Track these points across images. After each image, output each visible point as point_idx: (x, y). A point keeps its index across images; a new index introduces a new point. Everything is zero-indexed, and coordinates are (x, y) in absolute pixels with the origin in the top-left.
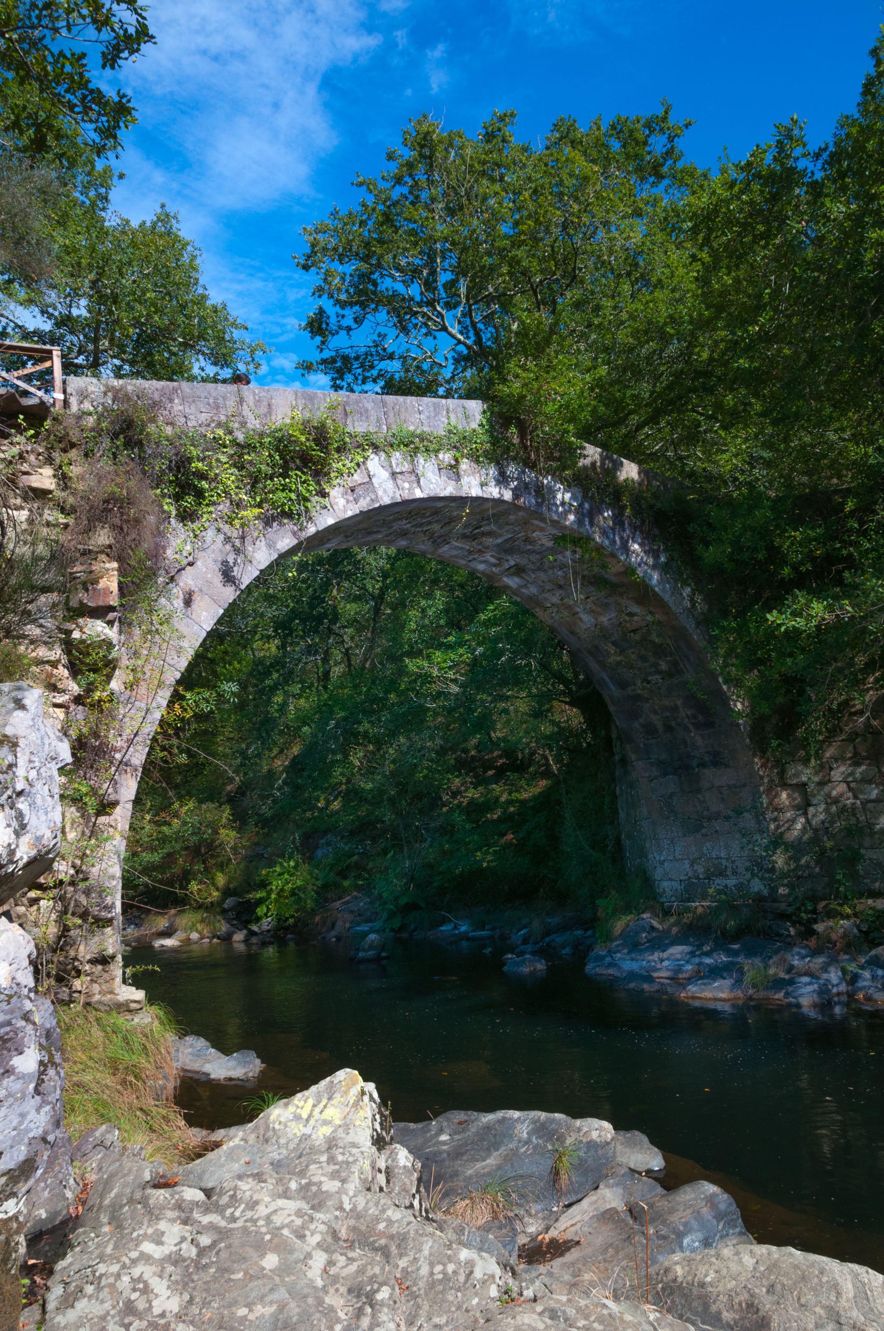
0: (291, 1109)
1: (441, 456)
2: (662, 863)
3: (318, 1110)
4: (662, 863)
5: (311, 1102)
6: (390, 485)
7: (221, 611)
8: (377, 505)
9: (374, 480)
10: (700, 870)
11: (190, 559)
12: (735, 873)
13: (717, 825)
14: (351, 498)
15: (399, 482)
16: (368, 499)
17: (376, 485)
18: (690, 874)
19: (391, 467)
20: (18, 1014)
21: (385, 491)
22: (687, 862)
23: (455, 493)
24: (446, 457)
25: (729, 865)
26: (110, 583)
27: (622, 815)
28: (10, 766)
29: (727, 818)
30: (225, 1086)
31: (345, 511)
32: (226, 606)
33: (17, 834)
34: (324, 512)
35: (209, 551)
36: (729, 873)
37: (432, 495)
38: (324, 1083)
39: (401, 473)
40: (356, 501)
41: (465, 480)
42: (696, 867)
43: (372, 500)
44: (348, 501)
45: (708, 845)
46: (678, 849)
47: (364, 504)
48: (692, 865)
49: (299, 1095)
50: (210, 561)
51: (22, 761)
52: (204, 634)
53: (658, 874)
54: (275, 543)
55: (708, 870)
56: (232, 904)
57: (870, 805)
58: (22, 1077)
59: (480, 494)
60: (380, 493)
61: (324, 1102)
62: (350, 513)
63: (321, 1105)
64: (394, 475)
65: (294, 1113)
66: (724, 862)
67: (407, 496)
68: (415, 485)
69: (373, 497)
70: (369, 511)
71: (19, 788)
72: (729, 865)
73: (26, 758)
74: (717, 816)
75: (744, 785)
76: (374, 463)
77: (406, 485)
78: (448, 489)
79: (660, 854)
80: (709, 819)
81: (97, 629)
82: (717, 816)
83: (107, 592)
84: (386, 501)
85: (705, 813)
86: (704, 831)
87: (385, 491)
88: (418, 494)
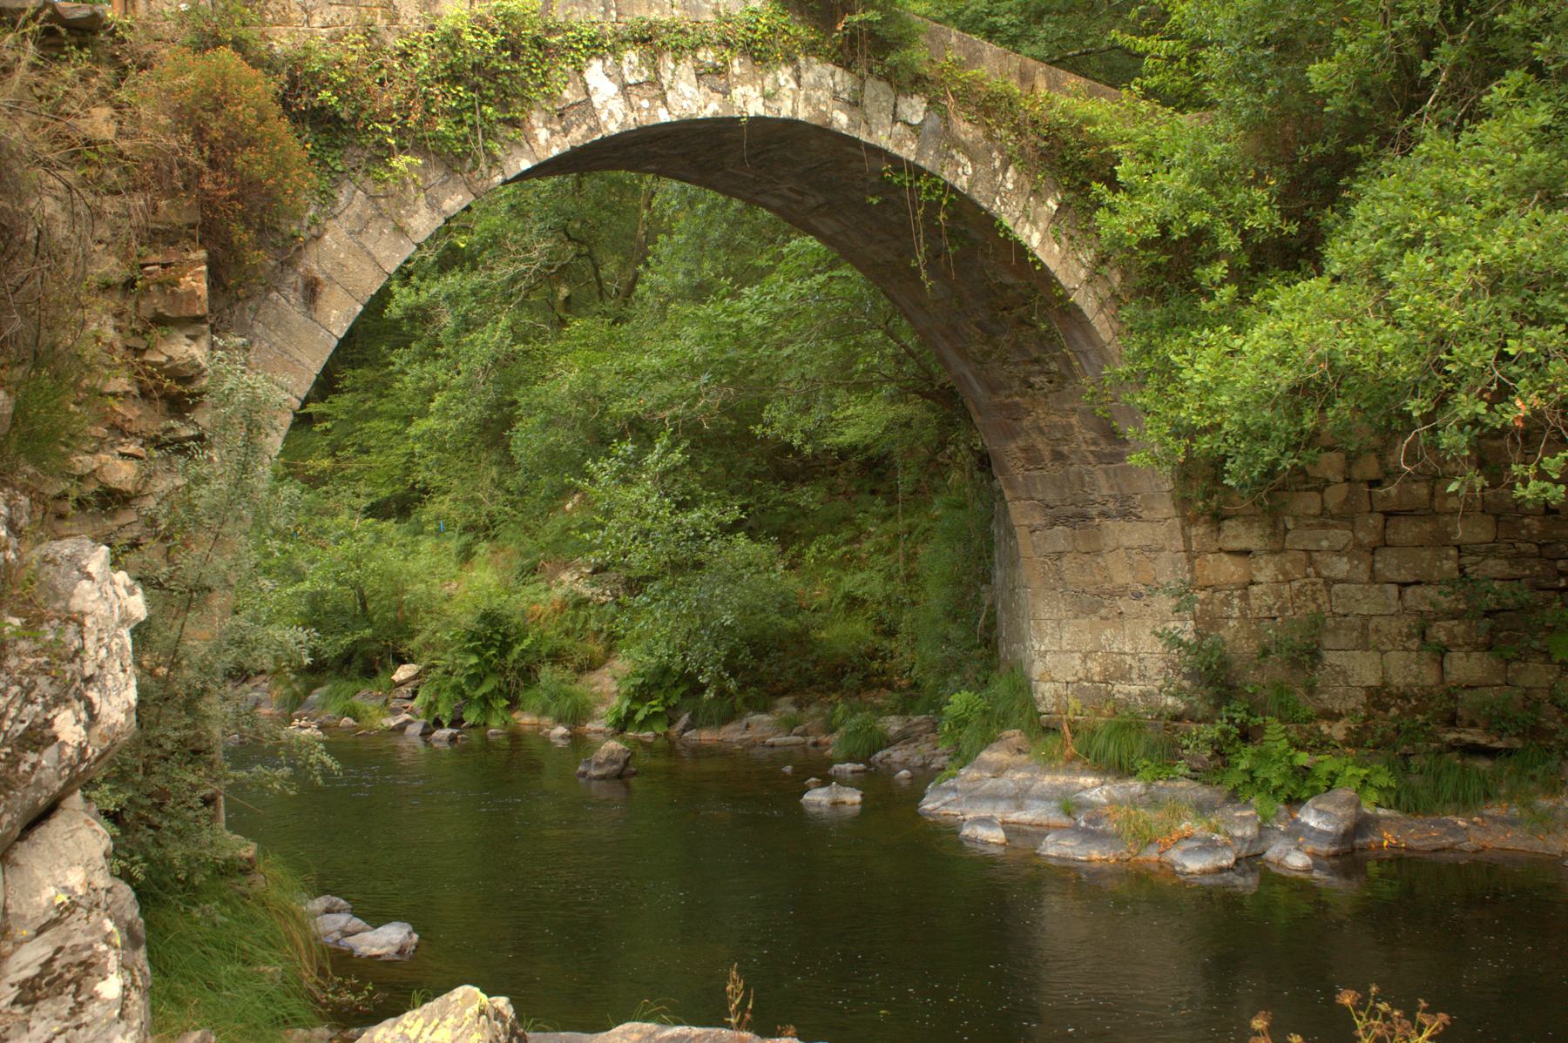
0: (399, 1029)
1: (701, 55)
2: (1043, 655)
3: (427, 1031)
4: (1043, 655)
5: (421, 1021)
6: (618, 106)
7: (360, 308)
8: (598, 137)
9: (594, 99)
10: (1095, 668)
11: (314, 231)
12: (1142, 676)
13: (1122, 604)
14: (558, 128)
15: (634, 99)
16: (585, 127)
17: (597, 105)
18: (1081, 675)
19: (621, 75)
20: (98, 936)
21: (611, 114)
22: (1077, 655)
23: (721, 113)
24: (707, 56)
25: (1135, 664)
26: (196, 282)
27: (999, 573)
28: (77, 652)
29: (1138, 596)
30: (389, 963)
31: (549, 147)
32: (367, 300)
33: (88, 728)
34: (516, 151)
35: (342, 218)
36: (1134, 676)
37: (685, 116)
38: (437, 1002)
39: (638, 85)
40: (566, 131)
41: (737, 92)
42: (1089, 664)
43: (590, 129)
44: (553, 133)
45: (1108, 632)
46: (1066, 636)
47: (578, 136)
48: (1084, 661)
49: (408, 1014)
50: (343, 233)
51: (90, 643)
52: (335, 343)
53: (1037, 669)
54: (439, 202)
55: (1106, 669)
56: (410, 674)
57: (1337, 587)
58: (107, 1002)
59: (761, 112)
60: (604, 117)
61: (436, 1021)
62: (555, 152)
63: (432, 1027)
64: (624, 88)
65: (402, 1034)
66: (1129, 659)
67: (645, 119)
68: (659, 103)
69: (592, 124)
70: (585, 147)
71: (88, 672)
72: (1135, 664)
73: (94, 638)
74: (1122, 592)
75: (1162, 549)
76: (595, 73)
77: (645, 103)
78: (711, 108)
79: (1041, 641)
80: (1112, 595)
81: (184, 349)
82: (1122, 592)
83: (192, 295)
84: (613, 129)
85: (1106, 585)
86: (1103, 612)
87: (611, 114)
88: (663, 116)
